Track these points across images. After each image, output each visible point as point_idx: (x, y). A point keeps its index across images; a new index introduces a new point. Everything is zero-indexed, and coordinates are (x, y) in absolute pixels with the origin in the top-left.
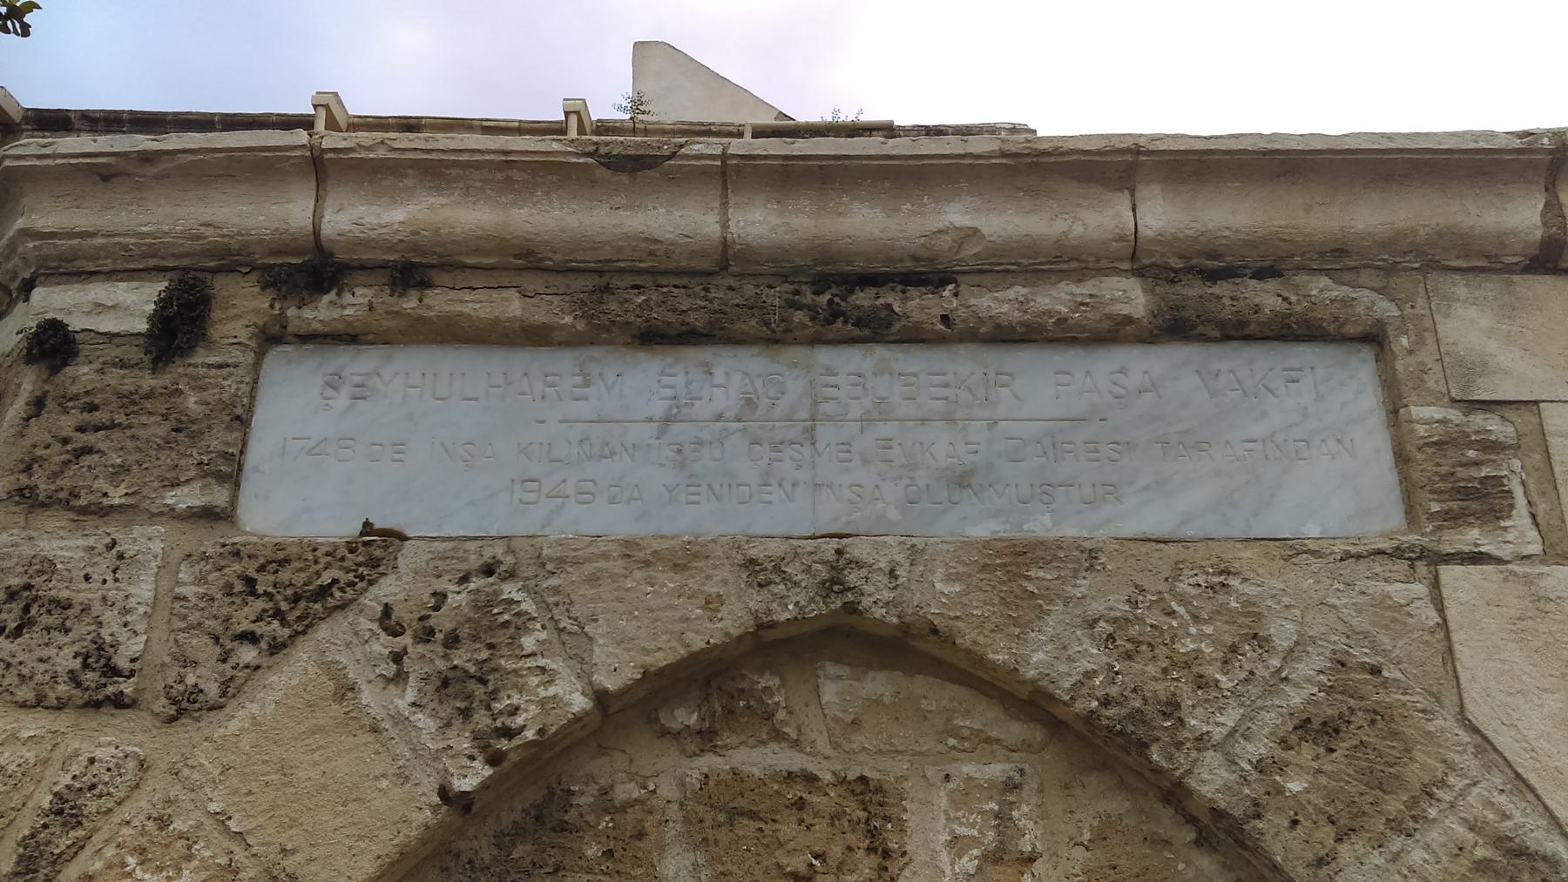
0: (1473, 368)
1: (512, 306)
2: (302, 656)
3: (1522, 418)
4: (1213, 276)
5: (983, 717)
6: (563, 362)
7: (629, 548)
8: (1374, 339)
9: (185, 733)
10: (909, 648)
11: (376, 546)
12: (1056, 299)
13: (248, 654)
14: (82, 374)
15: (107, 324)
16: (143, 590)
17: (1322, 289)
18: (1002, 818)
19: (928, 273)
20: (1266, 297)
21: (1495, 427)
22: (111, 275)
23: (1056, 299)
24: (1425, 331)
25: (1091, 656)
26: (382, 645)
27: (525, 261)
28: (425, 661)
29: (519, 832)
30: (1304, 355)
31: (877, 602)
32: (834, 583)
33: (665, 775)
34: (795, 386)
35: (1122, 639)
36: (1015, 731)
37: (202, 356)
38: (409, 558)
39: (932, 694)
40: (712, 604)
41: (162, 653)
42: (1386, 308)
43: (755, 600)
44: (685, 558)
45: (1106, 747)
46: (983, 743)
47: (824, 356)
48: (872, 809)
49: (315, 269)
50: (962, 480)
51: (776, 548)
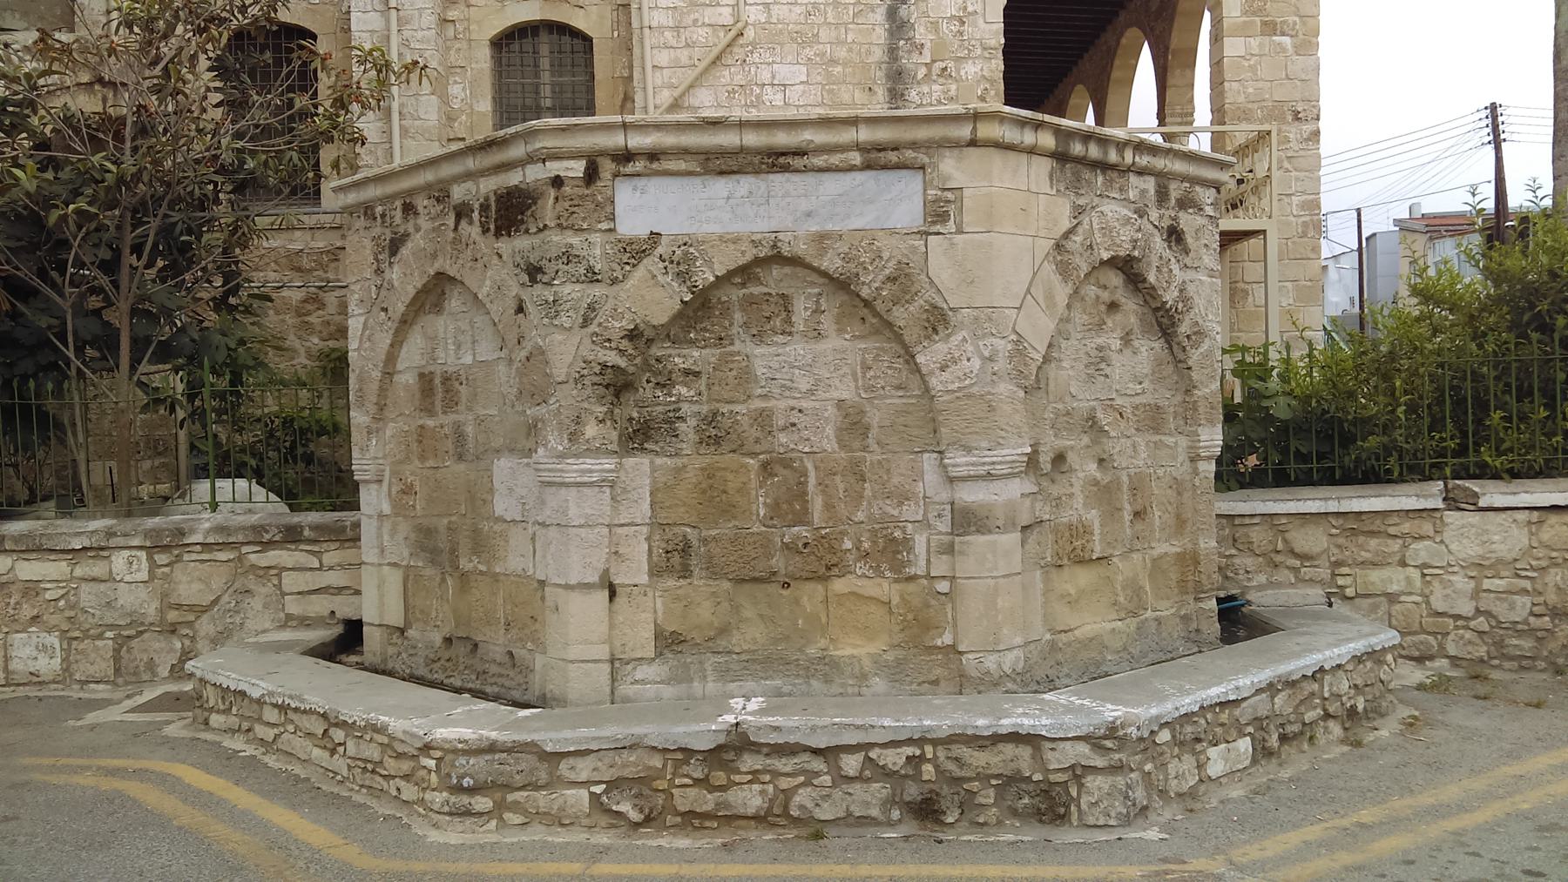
0: (949, 178)
1: (682, 165)
2: (641, 267)
3: (958, 193)
4: (880, 150)
5: (814, 277)
6: (697, 181)
7: (721, 238)
8: (922, 168)
9: (615, 287)
10: (795, 261)
11: (655, 236)
12: (835, 159)
13: (628, 268)
14: (567, 189)
15: (571, 174)
16: (598, 252)
17: (910, 154)
18: (817, 302)
19: (800, 153)
20: (893, 157)
21: (950, 196)
22: (569, 158)
23: (835, 159)
24: (935, 166)
25: (839, 263)
26: (661, 265)
27: (684, 152)
28: (673, 269)
29: (698, 309)
30: (904, 172)
31: (786, 251)
32: (774, 246)
33: (735, 294)
34: (763, 186)
35: (847, 258)
36: (822, 280)
37: (599, 184)
38: (664, 240)
39: (800, 272)
40: (743, 253)
41: (606, 268)
42: (926, 160)
43: (754, 251)
44: (736, 241)
45: (841, 284)
46: (813, 284)
47: (771, 176)
48: (785, 301)
49: (626, 156)
50: (809, 214)
51: (759, 236)
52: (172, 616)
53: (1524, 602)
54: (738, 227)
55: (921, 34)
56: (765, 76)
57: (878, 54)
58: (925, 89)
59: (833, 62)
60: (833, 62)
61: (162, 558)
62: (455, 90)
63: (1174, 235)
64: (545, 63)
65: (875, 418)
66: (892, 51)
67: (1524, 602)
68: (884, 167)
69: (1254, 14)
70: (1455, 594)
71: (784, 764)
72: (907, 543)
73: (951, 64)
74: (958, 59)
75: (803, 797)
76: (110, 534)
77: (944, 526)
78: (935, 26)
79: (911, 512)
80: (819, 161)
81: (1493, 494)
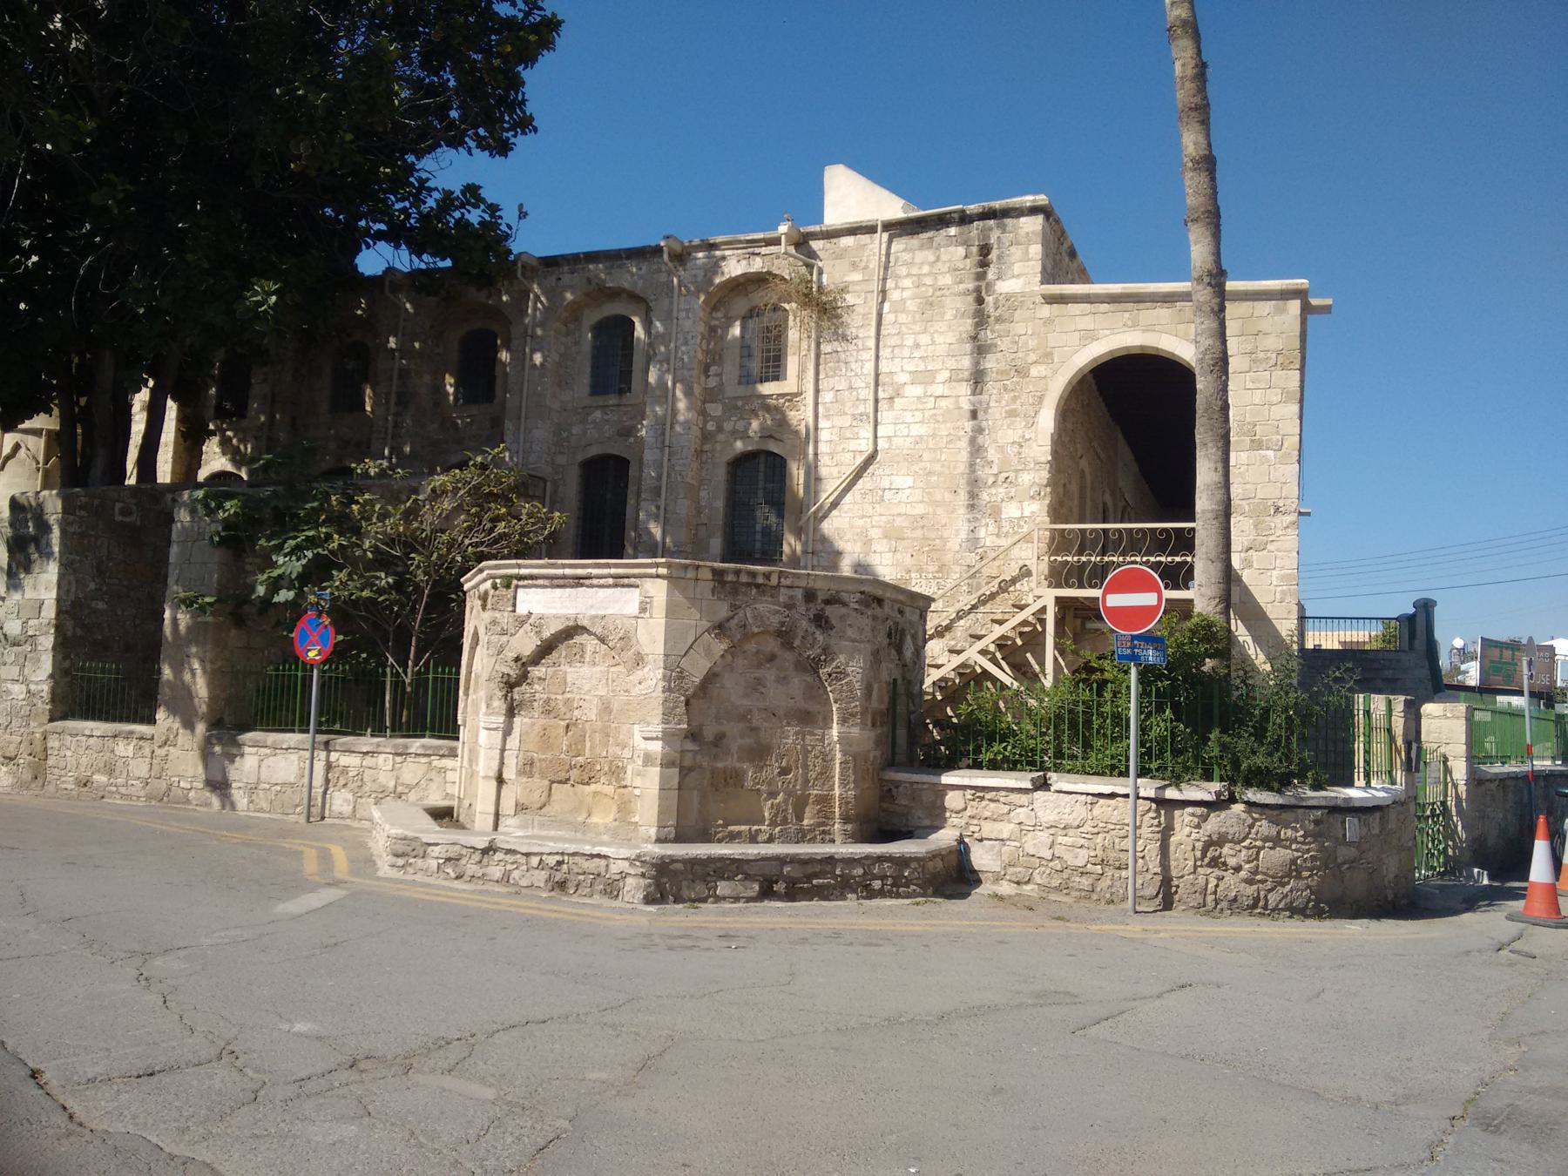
23: (602, 581)
52: (400, 789)
53: (1084, 854)
54: (563, 611)
55: (992, 454)
56: (886, 483)
57: (962, 468)
58: (993, 491)
59: (930, 473)
60: (930, 473)
61: (399, 759)
62: (703, 494)
63: (821, 621)
64: (761, 476)
65: (615, 706)
66: (972, 465)
67: (1084, 854)
68: (623, 586)
69: (1244, 434)
70: (1038, 843)
71: (509, 858)
72: (624, 769)
73: (1012, 475)
74: (1017, 471)
75: (516, 874)
76: (378, 745)
77: (640, 762)
78: (1001, 449)
79: (627, 753)
80: (595, 582)
81: (1058, 781)
